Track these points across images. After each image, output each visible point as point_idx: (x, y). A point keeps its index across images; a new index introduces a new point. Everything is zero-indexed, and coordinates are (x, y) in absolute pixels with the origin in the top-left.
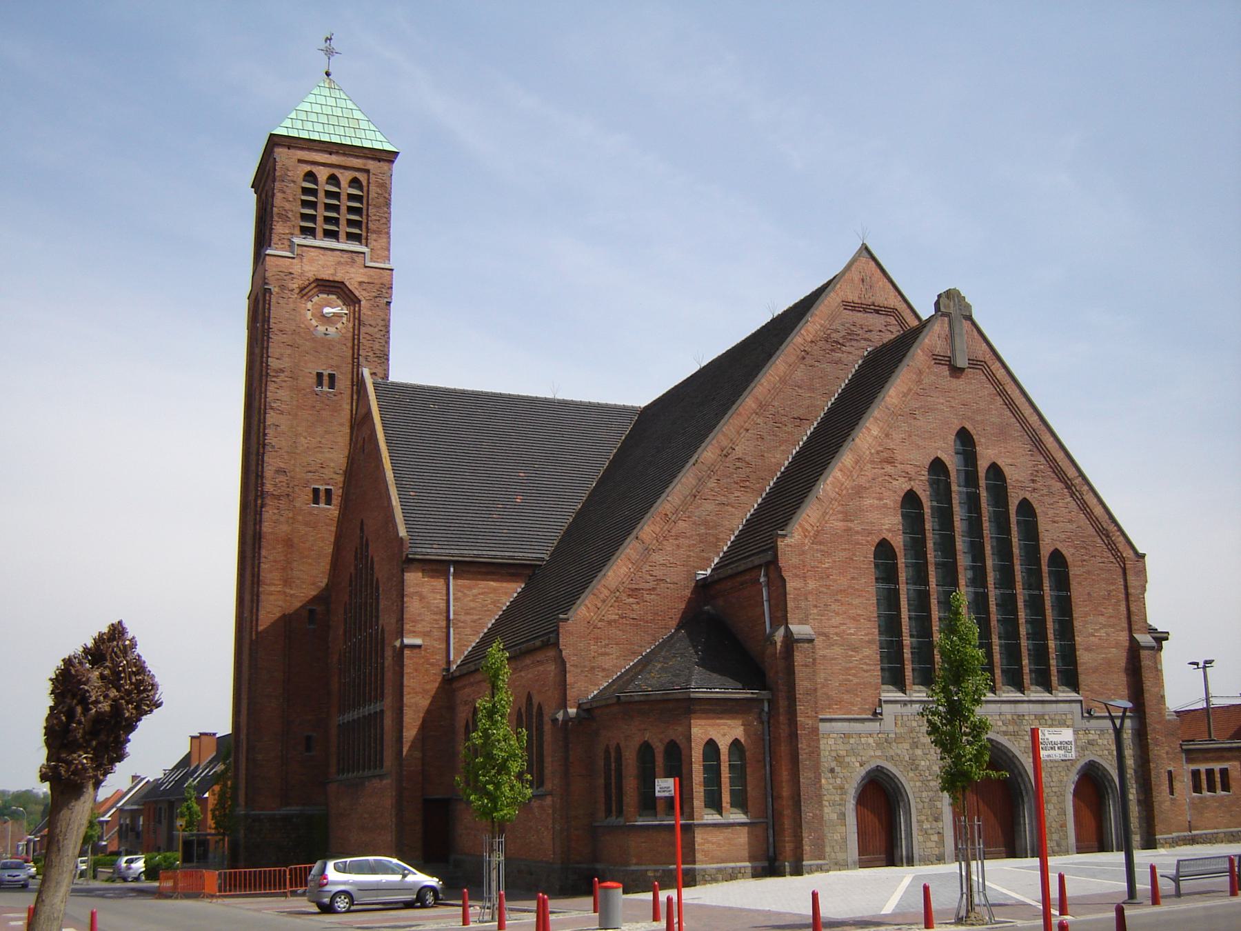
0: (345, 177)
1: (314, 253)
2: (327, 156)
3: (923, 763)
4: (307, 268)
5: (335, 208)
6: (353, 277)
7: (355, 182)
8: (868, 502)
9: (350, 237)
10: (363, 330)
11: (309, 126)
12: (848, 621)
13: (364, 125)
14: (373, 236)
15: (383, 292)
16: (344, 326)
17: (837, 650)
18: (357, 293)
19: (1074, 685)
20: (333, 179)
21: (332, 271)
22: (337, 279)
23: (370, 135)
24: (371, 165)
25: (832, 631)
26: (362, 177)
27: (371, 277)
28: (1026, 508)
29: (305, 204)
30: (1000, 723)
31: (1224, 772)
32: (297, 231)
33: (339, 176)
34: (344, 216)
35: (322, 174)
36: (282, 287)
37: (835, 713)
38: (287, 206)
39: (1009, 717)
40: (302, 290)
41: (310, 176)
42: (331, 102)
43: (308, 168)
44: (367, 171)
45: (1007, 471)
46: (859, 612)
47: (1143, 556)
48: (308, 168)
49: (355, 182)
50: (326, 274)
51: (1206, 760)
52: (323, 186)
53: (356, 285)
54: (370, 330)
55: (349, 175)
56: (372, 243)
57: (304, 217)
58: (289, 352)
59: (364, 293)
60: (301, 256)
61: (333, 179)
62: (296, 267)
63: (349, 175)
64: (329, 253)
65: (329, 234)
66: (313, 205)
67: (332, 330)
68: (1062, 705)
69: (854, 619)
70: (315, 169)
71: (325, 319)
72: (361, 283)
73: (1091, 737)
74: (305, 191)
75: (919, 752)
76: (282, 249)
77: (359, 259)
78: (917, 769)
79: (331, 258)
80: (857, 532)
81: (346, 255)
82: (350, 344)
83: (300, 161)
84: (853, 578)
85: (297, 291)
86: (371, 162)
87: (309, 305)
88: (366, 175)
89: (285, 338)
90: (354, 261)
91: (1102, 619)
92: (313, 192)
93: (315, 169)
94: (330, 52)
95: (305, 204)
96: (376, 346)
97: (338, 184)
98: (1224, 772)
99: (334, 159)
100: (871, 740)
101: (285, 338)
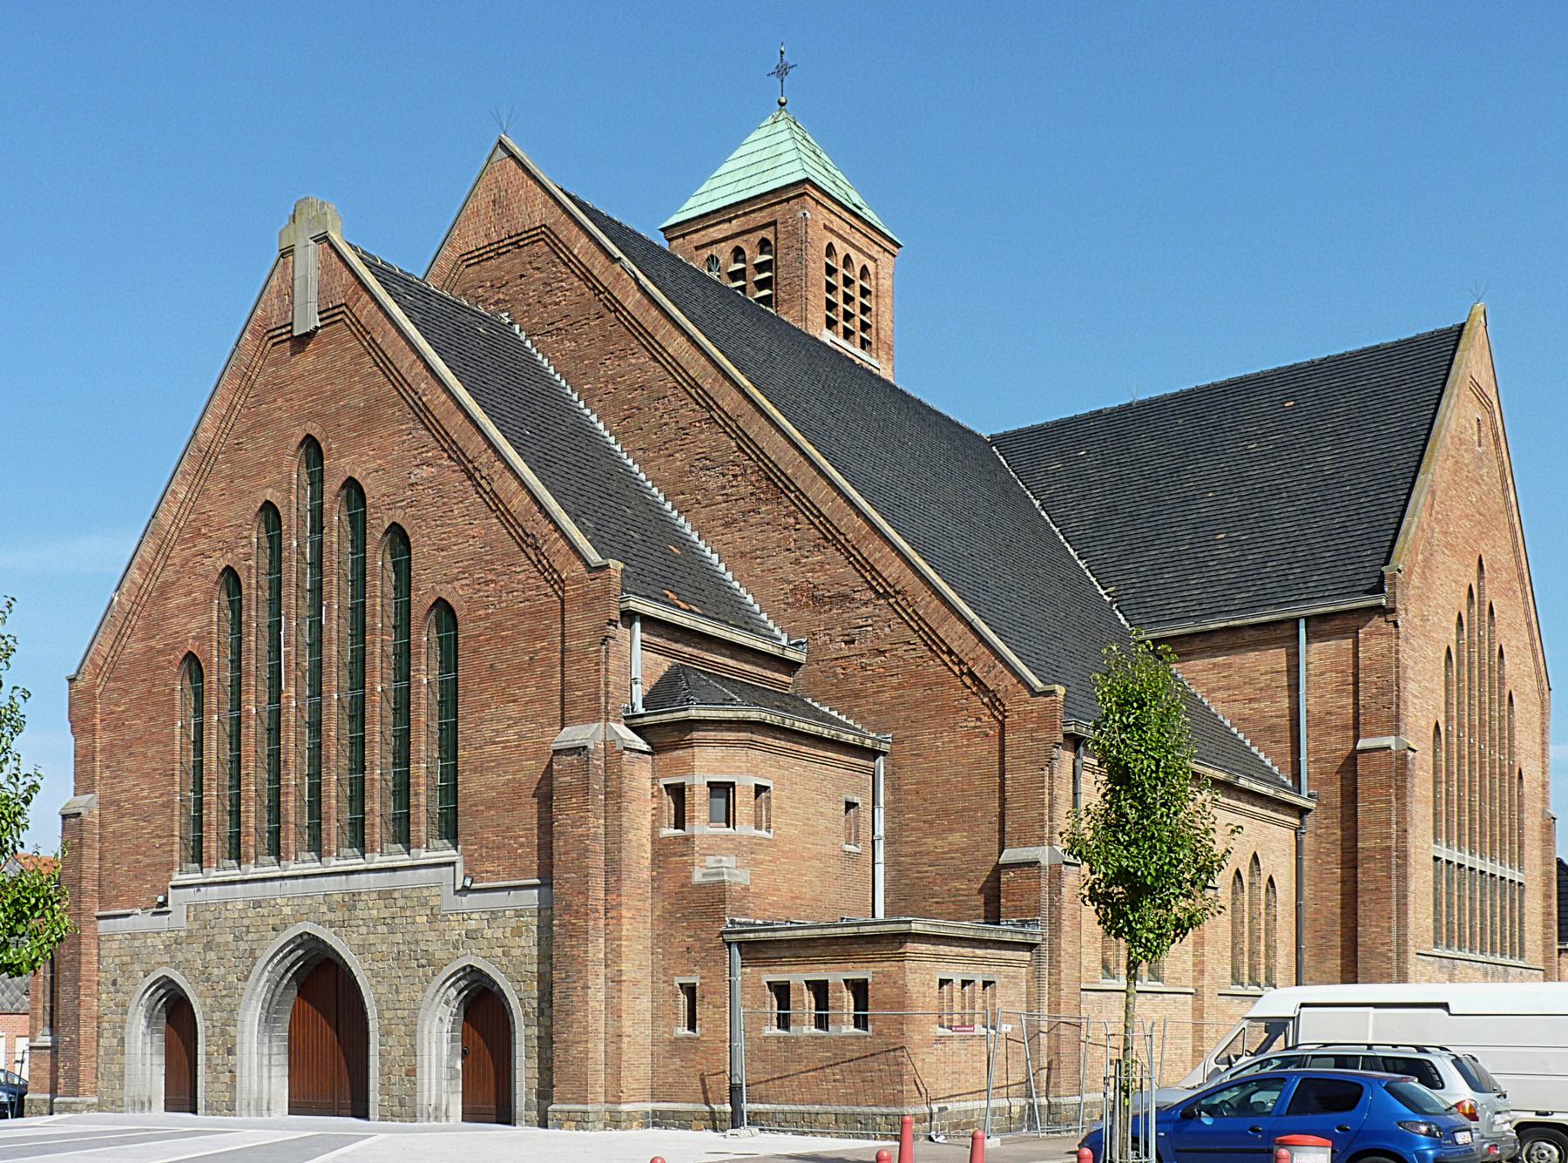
0: (749, 244)
2: (726, 226)
3: (216, 971)
7: (764, 245)
8: (173, 603)
12: (141, 780)
17: (128, 821)
19: (450, 830)
25: (123, 796)
26: (768, 234)
28: (398, 537)
30: (324, 909)
31: (1436, 945)
37: (116, 907)
39: (338, 898)
45: (367, 484)
46: (155, 765)
48: (706, 253)
49: (764, 245)
51: (847, 957)
61: (738, 253)
68: (422, 871)
69: (146, 775)
70: (713, 250)
73: (473, 925)
75: (212, 955)
78: (208, 980)
80: (160, 652)
84: (151, 719)
91: (513, 710)
98: (1436, 945)
99: (735, 226)
100: (158, 942)
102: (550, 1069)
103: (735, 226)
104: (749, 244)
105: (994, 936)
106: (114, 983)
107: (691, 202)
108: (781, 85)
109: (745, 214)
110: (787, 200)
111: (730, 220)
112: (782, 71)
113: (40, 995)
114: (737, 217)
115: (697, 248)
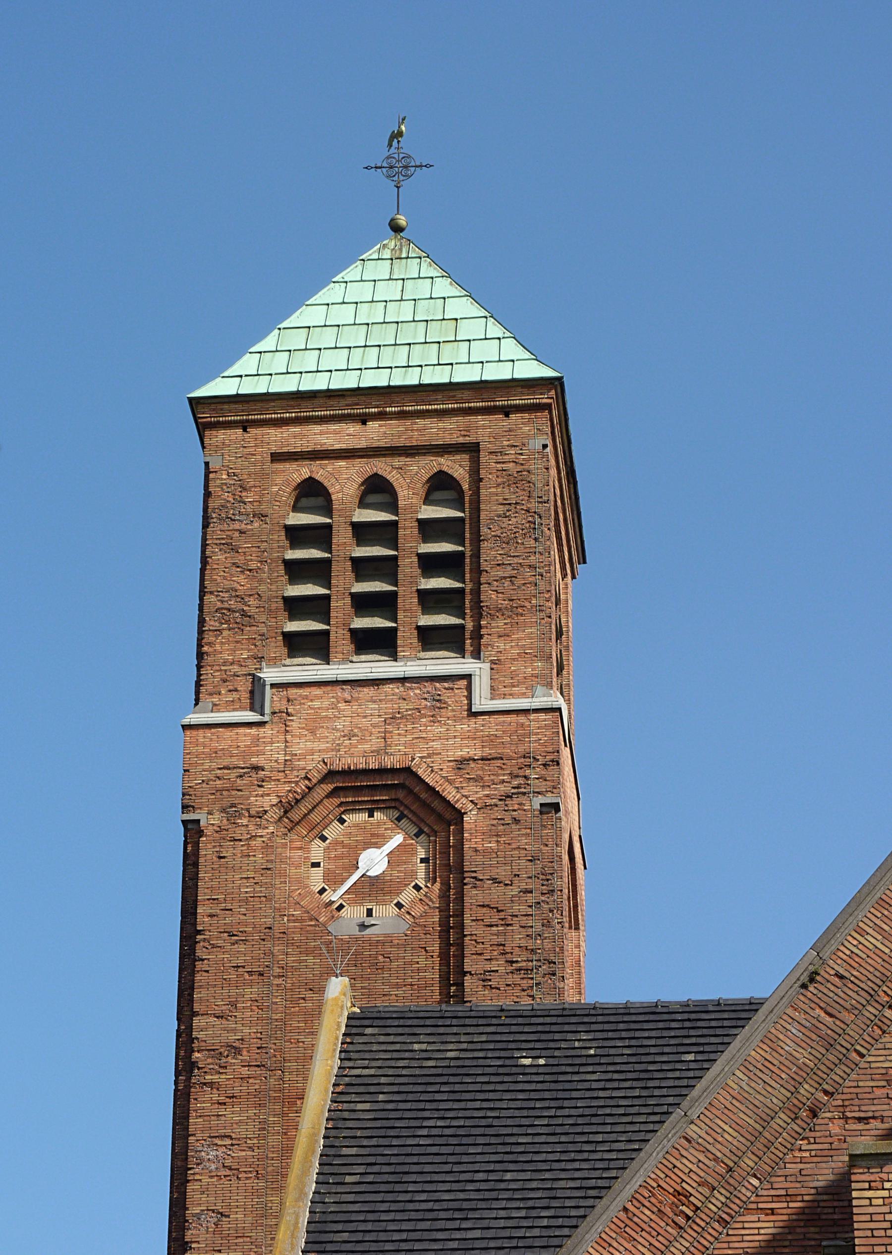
0: (408, 479)
1: (321, 700)
2: (353, 428)
4: (300, 746)
5: (386, 568)
6: (436, 750)
7: (440, 486)
9: (430, 638)
10: (472, 896)
11: (309, 361)
13: (471, 329)
14: (493, 626)
15: (529, 768)
16: (418, 892)
18: (451, 794)
20: (377, 489)
21: (375, 742)
22: (389, 762)
23: (489, 350)
24: (484, 429)
26: (457, 468)
27: (491, 740)
29: (297, 571)
32: (277, 648)
33: (393, 477)
34: (414, 581)
35: (344, 481)
36: (232, 812)
38: (242, 582)
40: (287, 808)
41: (312, 493)
42: (392, 291)
43: (301, 472)
44: (472, 449)
47: (364, 423)
48: (301, 472)
49: (440, 486)
50: (358, 755)
52: (349, 506)
53: (447, 770)
54: (495, 894)
55: (424, 468)
56: (494, 645)
57: (295, 607)
58: (250, 992)
59: (477, 792)
60: (283, 716)
61: (377, 489)
62: (272, 753)
63: (424, 468)
64: (367, 692)
65: (380, 643)
66: (319, 571)
67: (385, 913)
70: (321, 471)
71: (372, 888)
72: (461, 763)
74: (297, 535)
76: (231, 706)
77: (455, 697)
79: (372, 707)
81: (415, 691)
82: (435, 948)
83: (277, 457)
85: (274, 814)
86: (481, 420)
87: (317, 850)
88: (464, 459)
89: (242, 954)
90: (439, 703)
92: (320, 536)
93: (321, 471)
94: (399, 169)
95: (297, 571)
96: (517, 938)
97: (392, 506)
99: (375, 433)
101: (242, 954)
102: (196, 864)
103: (375, 433)
104: (408, 479)
105: (567, 857)
106: (508, 985)
107: (247, 363)
108: (397, 194)
109: (402, 415)
110: (507, 411)
111: (364, 420)
112: (399, 169)
113: (338, 360)
114: (381, 416)
115: (277, 457)
